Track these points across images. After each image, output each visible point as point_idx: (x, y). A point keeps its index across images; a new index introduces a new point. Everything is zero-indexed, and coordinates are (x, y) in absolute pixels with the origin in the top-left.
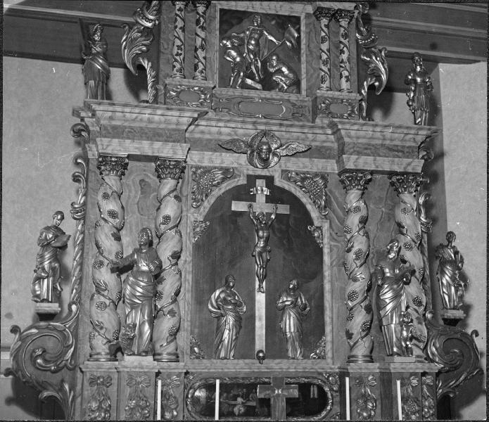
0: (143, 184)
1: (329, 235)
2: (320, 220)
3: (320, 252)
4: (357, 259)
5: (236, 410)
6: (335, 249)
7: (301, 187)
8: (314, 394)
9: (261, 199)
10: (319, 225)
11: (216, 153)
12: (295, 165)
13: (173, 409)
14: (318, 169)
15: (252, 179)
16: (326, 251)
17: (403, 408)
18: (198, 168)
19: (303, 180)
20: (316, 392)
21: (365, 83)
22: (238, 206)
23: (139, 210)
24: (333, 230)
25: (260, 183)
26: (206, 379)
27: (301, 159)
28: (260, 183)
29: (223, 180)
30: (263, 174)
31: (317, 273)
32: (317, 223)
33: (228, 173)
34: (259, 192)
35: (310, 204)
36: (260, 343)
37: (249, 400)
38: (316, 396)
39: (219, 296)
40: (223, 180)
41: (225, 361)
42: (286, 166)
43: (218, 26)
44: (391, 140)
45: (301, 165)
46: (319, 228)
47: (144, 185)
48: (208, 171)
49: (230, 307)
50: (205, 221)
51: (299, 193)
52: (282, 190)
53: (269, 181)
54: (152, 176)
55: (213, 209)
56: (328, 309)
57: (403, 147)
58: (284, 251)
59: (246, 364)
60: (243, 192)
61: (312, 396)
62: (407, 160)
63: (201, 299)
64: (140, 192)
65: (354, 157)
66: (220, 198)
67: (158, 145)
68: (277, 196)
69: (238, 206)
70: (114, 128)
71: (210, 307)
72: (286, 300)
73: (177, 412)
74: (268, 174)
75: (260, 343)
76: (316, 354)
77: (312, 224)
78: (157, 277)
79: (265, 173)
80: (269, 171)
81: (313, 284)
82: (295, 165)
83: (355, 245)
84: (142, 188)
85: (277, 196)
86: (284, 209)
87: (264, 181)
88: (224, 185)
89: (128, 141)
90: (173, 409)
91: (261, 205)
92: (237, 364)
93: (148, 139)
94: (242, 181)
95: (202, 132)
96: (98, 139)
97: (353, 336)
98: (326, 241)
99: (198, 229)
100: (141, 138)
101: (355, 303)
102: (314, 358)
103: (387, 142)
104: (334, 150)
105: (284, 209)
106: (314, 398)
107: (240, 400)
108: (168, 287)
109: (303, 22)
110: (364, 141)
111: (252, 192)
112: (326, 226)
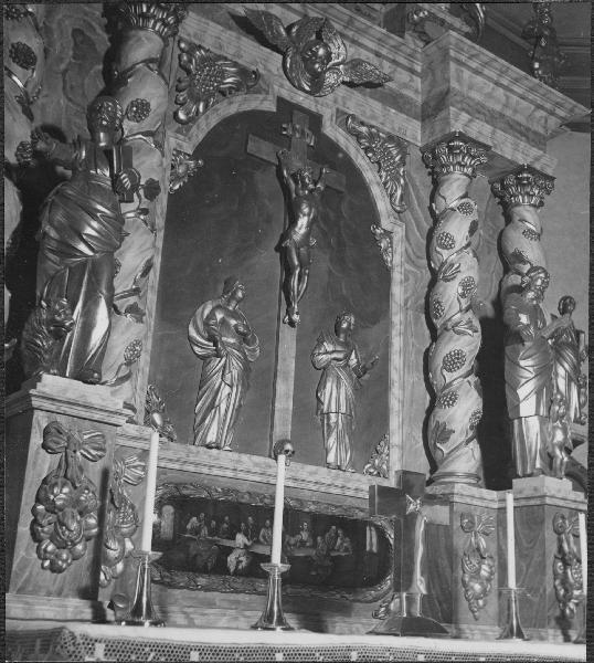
0: (80, 38)
1: (403, 249)
2: (392, 219)
3: (385, 274)
4: (463, 295)
5: (231, 559)
6: (411, 277)
7: (367, 150)
8: (371, 545)
10: (388, 228)
11: (229, 32)
13: (124, 536)
14: (393, 129)
16: (397, 276)
17: (578, 543)
18: (193, 48)
19: (372, 137)
20: (375, 540)
23: (64, 88)
24: (410, 244)
26: (177, 486)
27: (371, 101)
29: (237, 88)
31: (375, 309)
32: (386, 223)
34: (297, 135)
35: (378, 184)
36: (283, 426)
37: (258, 542)
38: (375, 549)
39: (212, 315)
40: (237, 88)
41: (214, 451)
42: (344, 103)
44: (516, 111)
45: (368, 113)
46: (388, 234)
47: (82, 43)
48: (211, 60)
49: (232, 341)
50: (194, 157)
54: (99, 31)
56: (396, 385)
57: (528, 129)
58: (331, 260)
59: (256, 465)
61: (368, 548)
62: (535, 152)
64: (71, 53)
65: (465, 117)
71: (193, 333)
72: (328, 352)
73: (133, 544)
74: (313, 109)
75: (283, 426)
76: (373, 466)
77: (378, 224)
80: (317, 102)
81: (373, 332)
83: (462, 268)
84: (76, 44)
88: (239, 98)
90: (124, 536)
92: (239, 461)
97: (453, 437)
99: (181, 170)
101: (455, 375)
102: (371, 473)
103: (508, 113)
104: (416, 106)
106: (371, 552)
107: (241, 539)
111: (285, 129)
112: (399, 233)
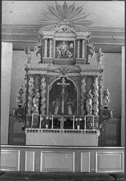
9: (63, 82)
12: (70, 75)
15: (62, 78)
21: (28, 110)
22: (59, 84)
25: (63, 79)
28: (63, 79)
30: (64, 77)
33: (57, 77)
36: (63, 112)
43: (55, 45)
51: (72, 80)
52: (68, 80)
53: (66, 78)
55: (53, 84)
60: (60, 81)
63: (50, 102)
66: (55, 82)
67: (40, 72)
68: (67, 81)
69: (59, 84)
70: (32, 68)
78: (40, 98)
79: (65, 76)
82: (70, 75)
85: (67, 81)
86: (68, 84)
87: (26, 145)
89: (34, 71)
91: (64, 83)
93: (38, 70)
94: (60, 78)
95: (51, 68)
96: (77, 78)
98: (78, 91)
100: (37, 70)
103: (91, 69)
105: (68, 84)
108: (44, 100)
109: (74, 42)
110: (85, 69)
112: (78, 87)
